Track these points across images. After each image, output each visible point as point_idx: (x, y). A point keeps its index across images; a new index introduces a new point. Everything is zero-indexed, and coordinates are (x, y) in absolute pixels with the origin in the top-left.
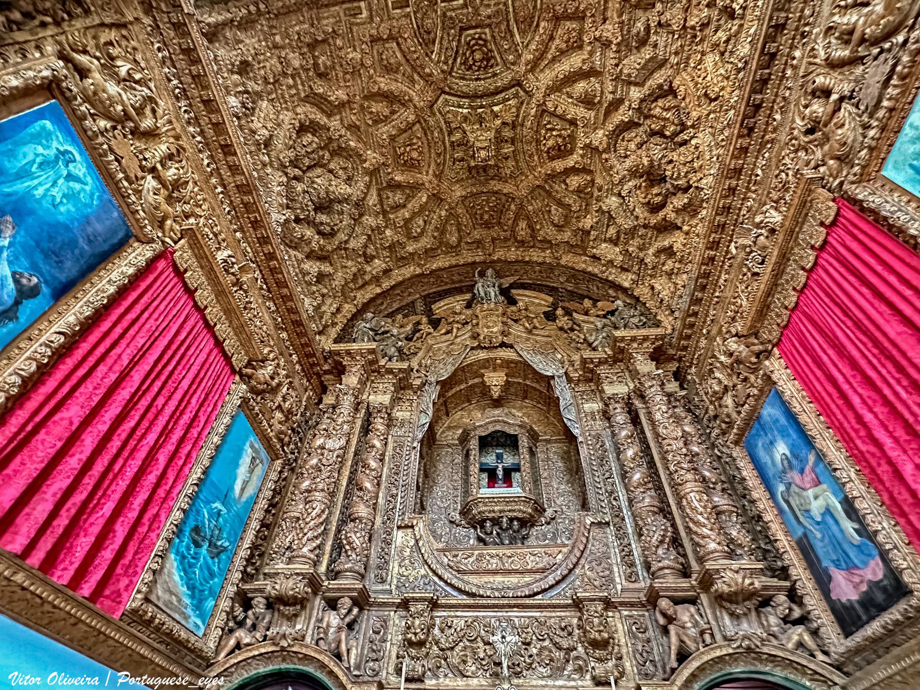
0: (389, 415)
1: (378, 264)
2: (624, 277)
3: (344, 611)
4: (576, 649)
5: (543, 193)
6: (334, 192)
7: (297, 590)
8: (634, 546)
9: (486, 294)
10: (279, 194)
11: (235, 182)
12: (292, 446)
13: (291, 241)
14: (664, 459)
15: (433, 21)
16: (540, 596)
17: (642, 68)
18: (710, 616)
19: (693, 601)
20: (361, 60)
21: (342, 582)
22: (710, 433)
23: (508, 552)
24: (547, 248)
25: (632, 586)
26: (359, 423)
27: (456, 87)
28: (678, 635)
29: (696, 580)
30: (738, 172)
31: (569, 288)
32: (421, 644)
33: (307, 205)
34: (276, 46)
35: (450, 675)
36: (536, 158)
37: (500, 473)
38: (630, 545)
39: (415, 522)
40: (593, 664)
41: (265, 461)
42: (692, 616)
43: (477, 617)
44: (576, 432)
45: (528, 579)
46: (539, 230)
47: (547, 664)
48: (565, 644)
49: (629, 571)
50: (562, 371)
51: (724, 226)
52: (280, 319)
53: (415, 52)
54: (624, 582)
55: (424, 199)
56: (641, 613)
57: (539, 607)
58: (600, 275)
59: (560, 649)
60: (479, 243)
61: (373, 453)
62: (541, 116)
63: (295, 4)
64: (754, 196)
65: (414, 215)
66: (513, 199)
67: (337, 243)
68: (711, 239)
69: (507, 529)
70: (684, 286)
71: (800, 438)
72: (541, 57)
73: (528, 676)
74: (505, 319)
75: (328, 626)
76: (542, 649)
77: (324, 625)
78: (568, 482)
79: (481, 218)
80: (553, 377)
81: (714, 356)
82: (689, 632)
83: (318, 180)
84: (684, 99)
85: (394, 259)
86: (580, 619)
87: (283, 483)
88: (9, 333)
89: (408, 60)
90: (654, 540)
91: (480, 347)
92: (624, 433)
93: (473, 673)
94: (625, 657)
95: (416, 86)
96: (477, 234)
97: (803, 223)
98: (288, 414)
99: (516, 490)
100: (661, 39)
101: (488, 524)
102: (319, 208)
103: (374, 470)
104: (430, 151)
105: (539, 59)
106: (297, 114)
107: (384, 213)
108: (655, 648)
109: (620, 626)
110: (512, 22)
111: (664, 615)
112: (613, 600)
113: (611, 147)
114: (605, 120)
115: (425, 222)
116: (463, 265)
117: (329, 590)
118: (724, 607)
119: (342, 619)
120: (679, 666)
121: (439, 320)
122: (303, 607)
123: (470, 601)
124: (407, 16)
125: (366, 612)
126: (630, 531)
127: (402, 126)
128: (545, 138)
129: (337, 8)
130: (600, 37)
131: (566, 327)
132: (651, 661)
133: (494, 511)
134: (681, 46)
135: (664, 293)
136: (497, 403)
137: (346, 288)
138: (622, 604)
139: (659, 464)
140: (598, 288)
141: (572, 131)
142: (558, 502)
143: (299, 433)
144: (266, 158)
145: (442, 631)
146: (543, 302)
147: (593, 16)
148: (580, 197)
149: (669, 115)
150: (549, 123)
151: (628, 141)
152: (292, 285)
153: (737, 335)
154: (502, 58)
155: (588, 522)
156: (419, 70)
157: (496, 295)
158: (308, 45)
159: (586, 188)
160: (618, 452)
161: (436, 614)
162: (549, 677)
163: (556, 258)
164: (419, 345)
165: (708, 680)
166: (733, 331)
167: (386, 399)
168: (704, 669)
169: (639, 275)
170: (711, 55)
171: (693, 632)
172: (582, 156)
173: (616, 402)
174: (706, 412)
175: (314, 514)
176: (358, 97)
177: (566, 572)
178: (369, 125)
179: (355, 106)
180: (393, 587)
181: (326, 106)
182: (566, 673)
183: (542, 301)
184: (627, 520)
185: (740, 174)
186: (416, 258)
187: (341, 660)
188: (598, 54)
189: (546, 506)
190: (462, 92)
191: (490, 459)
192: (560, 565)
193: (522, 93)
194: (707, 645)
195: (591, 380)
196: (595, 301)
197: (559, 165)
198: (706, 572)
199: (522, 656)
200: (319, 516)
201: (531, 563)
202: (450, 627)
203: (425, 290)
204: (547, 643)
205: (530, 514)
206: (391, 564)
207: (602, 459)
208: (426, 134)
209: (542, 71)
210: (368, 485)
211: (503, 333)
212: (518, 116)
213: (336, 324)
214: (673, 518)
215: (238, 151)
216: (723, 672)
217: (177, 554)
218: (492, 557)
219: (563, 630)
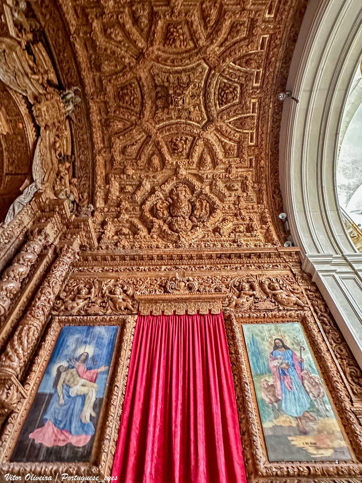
2: (101, 202)
31: (76, 163)
36: (167, 133)
64: (193, 270)
65: (127, 35)
66: (140, 118)
71: (107, 356)
72: (223, 135)
81: (100, 283)
91: (29, 106)
96: (109, 88)
97: (205, 302)
105: (221, 133)
110: (240, 116)
115: (120, 42)
140: (84, 184)
146: (65, 148)
151: (185, 190)
166: (125, 288)
169: (108, 212)
195: (43, 211)
208: (186, 52)
209: (215, 134)
211: (46, 127)
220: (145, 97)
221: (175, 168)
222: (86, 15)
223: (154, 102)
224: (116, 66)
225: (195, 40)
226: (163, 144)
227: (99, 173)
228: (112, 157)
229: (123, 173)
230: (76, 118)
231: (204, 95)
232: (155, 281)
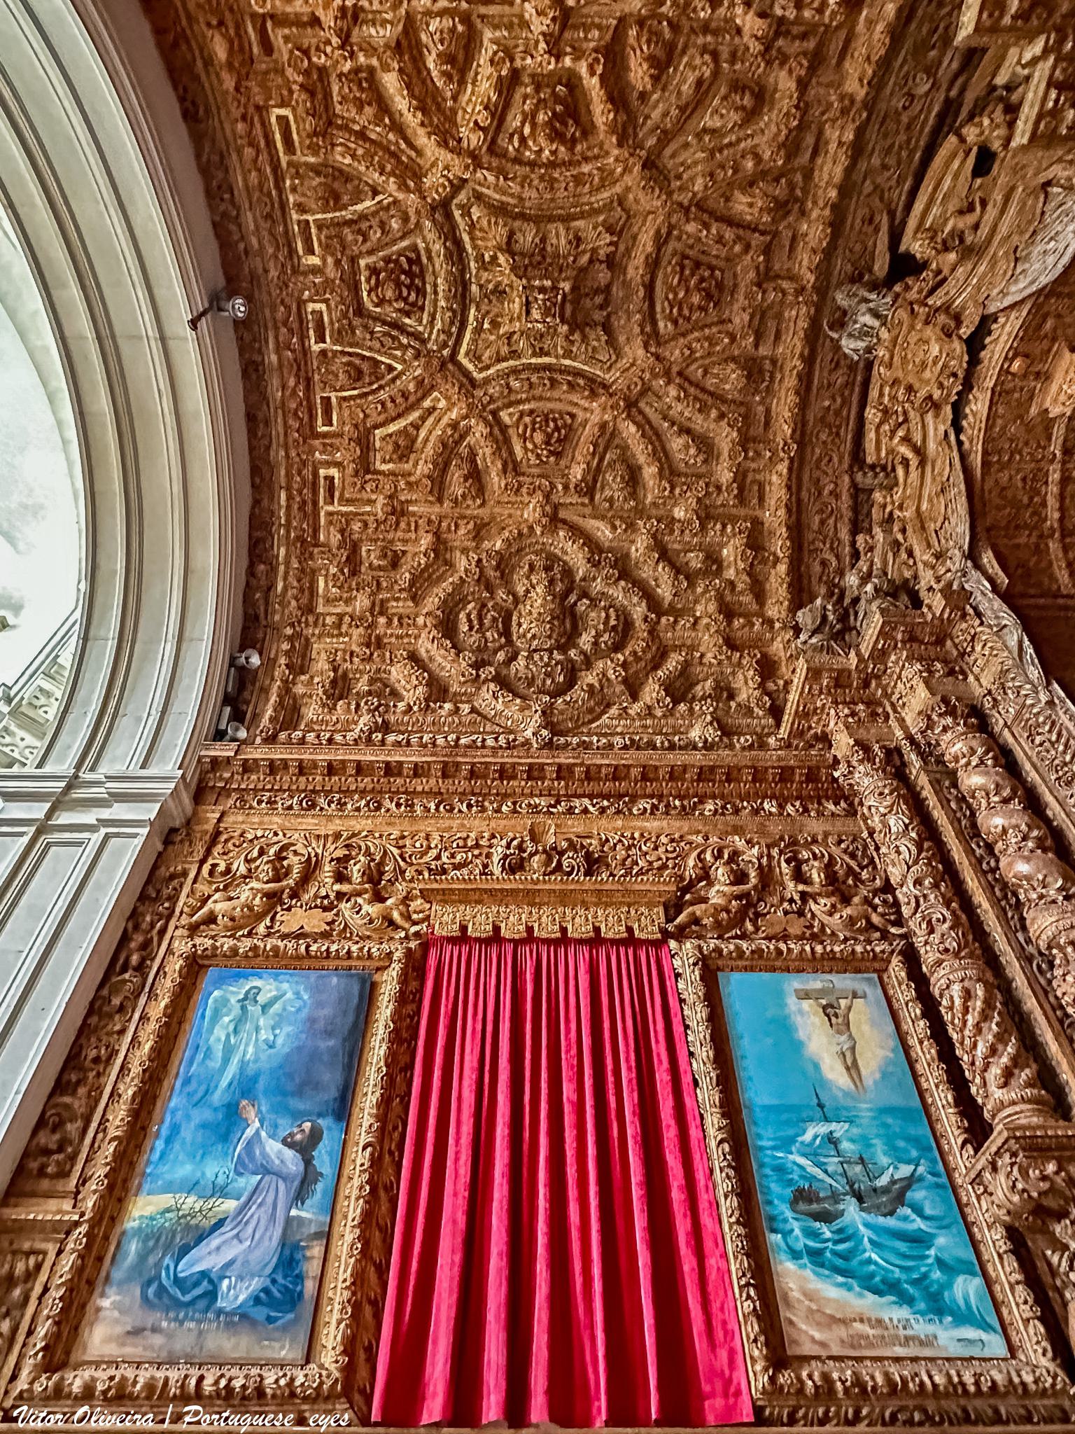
13: (591, 711)
27: (442, 337)
31: (955, 65)
36: (586, 168)
65: (661, 454)
66: (671, 228)
74: (922, 311)
88: (324, 1192)
96: (740, 319)
102: (568, 640)
154: (402, 238)
156: (412, 399)
163: (844, 112)
188: (373, 31)
190: (452, 323)
197: (601, 114)
208: (520, 402)
217: (795, 1255)
220: (641, 293)
221: (568, 35)
227: (880, 27)
229: (781, 27)
231: (465, 285)
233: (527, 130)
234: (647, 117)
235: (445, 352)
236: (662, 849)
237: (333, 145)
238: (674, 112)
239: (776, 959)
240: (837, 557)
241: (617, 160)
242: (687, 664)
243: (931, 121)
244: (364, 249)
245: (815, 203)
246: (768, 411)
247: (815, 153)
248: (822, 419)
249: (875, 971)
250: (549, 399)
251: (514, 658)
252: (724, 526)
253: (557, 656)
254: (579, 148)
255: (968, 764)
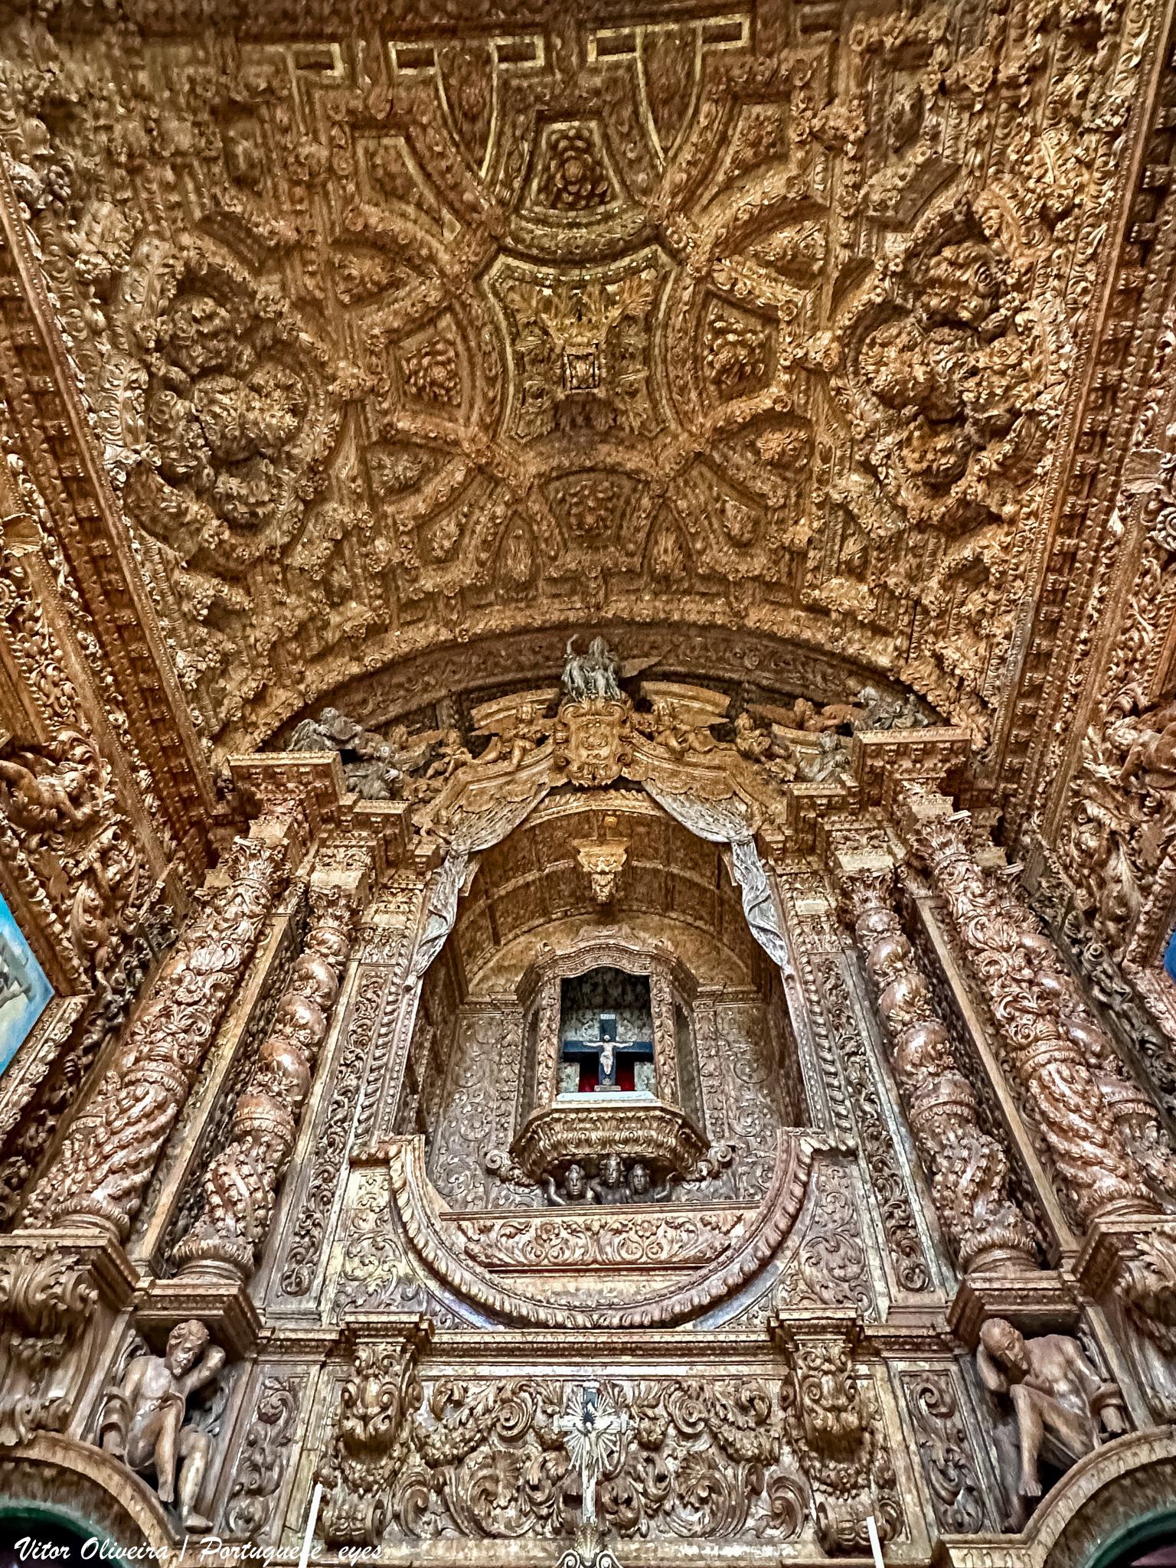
0: (354, 913)
1: (357, 612)
2: (880, 647)
3: (182, 1357)
4: (777, 1460)
5: (708, 474)
6: (256, 423)
7: (58, 1290)
8: (916, 1206)
9: (587, 682)
10: (128, 406)
11: (12, 337)
12: (119, 975)
13: (154, 519)
14: (983, 1000)
15: (484, 90)
16: (689, 1326)
17: (910, 187)
18: (1114, 1363)
19: (1069, 1327)
20: (330, 159)
21: (189, 1283)
22: (1081, 953)
23: (614, 1222)
24: (718, 595)
25: (914, 1299)
26: (280, 925)
27: (528, 237)
28: (1037, 1411)
29: (1074, 1271)
30: (1120, 347)
31: (765, 682)
32: (378, 1447)
33: (193, 446)
34: (139, 94)
35: (450, 1533)
36: (694, 395)
37: (607, 1062)
38: (906, 1201)
39: (393, 1150)
40: (820, 1498)
41: (37, 990)
42: (1070, 1363)
43: (530, 1377)
44: (778, 955)
45: (659, 1283)
46: (701, 553)
47: (703, 1501)
48: (748, 1445)
49: (906, 1263)
50: (747, 833)
51: (1094, 476)
52: (109, 679)
53: (442, 155)
54: (894, 1290)
55: (459, 477)
56: (937, 1366)
57: (686, 1351)
58: (828, 647)
59: (735, 1458)
60: (573, 581)
61: (308, 992)
62: (705, 306)
63: (185, 14)
64: (1160, 393)
65: (439, 509)
66: (647, 483)
67: (263, 546)
68: (1067, 510)
69: (617, 1185)
70: (1007, 637)
73: (652, 1535)
74: (626, 731)
75: (137, 1394)
76: (690, 1459)
77: (127, 1392)
78: (761, 1084)
79: (580, 526)
80: (727, 846)
81: (1083, 773)
82: (1065, 1405)
83: (225, 400)
84: (998, 234)
85: (393, 606)
86: (788, 1381)
87: (85, 1061)
89: (428, 176)
90: (964, 1181)
91: (570, 788)
92: (886, 950)
93: (508, 1526)
94: (902, 1479)
95: (446, 233)
96: (571, 560)
98: (113, 897)
99: (641, 1096)
100: (944, 121)
101: (575, 1174)
102: (224, 462)
103: (304, 1027)
104: (472, 374)
106: (182, 248)
107: (374, 501)
108: (979, 1456)
109: (887, 1400)
110: (644, 108)
111: (998, 1363)
112: (869, 1332)
113: (848, 362)
114: (834, 310)
115: (462, 528)
116: (541, 629)
117: (151, 1300)
118: (1151, 1336)
119: (178, 1379)
120: (1045, 1492)
121: (488, 739)
122: (73, 1342)
123: (514, 1337)
124: (429, 82)
125: (248, 1366)
126: (906, 1171)
127: (416, 311)
128: (712, 350)
129: (281, 49)
130: (822, 129)
131: (757, 749)
132: (970, 1490)
133: (588, 1142)
134: (988, 127)
135: (966, 665)
136: (607, 913)
137: (281, 652)
138: (892, 1342)
139: (968, 1012)
140: (824, 678)
141: (769, 338)
142: (738, 1129)
143: (140, 949)
144: (99, 317)
145: (437, 1414)
146: (709, 708)
147: (806, 86)
148: (784, 479)
149: (966, 276)
150: (720, 318)
151: (883, 345)
152: (142, 603)
153: (1135, 711)
154: (623, 182)
155: (808, 1150)
156: (452, 196)
157: (608, 685)
158: (213, 111)
159: (796, 458)
160: (873, 991)
161: (424, 1371)
162: (708, 1534)
163: (737, 614)
164: (437, 783)
165: (1119, 1533)
166: (1126, 703)
167: (350, 879)
168: (1108, 1502)
169: (910, 637)
170: (1052, 134)
171: (1073, 1404)
172: (789, 387)
173: (868, 887)
174: (1070, 907)
175: (135, 1112)
176: (319, 238)
177: (753, 1266)
178: (345, 306)
179: (313, 256)
180: (326, 1306)
181: (251, 250)
182: (750, 1523)
183: (709, 705)
184: (898, 1147)
185: (1127, 352)
186: (441, 605)
187: (155, 1485)
189: (710, 1136)
190: (542, 249)
191: (587, 1035)
192: (739, 1250)
193: (664, 258)
194: (1114, 1435)
195: (812, 850)
196: (819, 707)
197: (741, 409)
198: (1100, 1243)
199: (638, 1479)
200: (148, 1116)
201: (669, 1245)
202: (458, 1404)
203: (459, 681)
204: (703, 1445)
205: (673, 1150)
206: (326, 1248)
207: (837, 1016)
208: (465, 338)
209: (705, 208)
210: (287, 1060)
211: (622, 760)
212: (655, 304)
213: (255, 725)
214: (1009, 1133)
215: (21, 266)
216: (1160, 1510)
218: (573, 1232)
219: (744, 1409)
220: (588, 463)
222: (411, 604)
223: (605, 437)
224: (518, 537)
225: (431, 314)
226: (720, 414)
227: (794, 628)
228: (755, 579)
230: (647, 655)
231: (580, 263)
232: (1148, 579)
233: (731, 337)
234: (733, 449)
235: (509, 240)
236: (57, 691)
237: (716, 102)
238: (741, 476)
239: (21, 893)
240: (372, 712)
241: (702, 425)
242: (242, 613)
243: (727, 675)
244: (611, 131)
245: (667, 602)
246: (491, 604)
247: (703, 595)
248: (490, 653)
249: (56, 989)
250: (472, 374)
251: (181, 392)
252: (379, 597)
253: (204, 454)
254: (712, 388)
255: (326, 956)
